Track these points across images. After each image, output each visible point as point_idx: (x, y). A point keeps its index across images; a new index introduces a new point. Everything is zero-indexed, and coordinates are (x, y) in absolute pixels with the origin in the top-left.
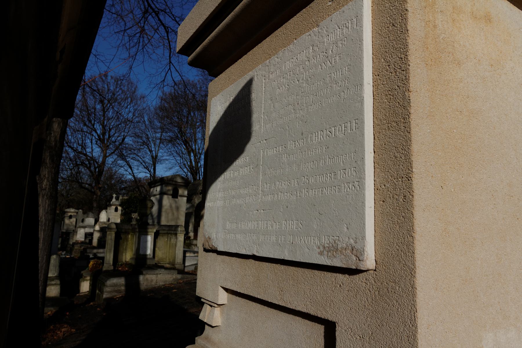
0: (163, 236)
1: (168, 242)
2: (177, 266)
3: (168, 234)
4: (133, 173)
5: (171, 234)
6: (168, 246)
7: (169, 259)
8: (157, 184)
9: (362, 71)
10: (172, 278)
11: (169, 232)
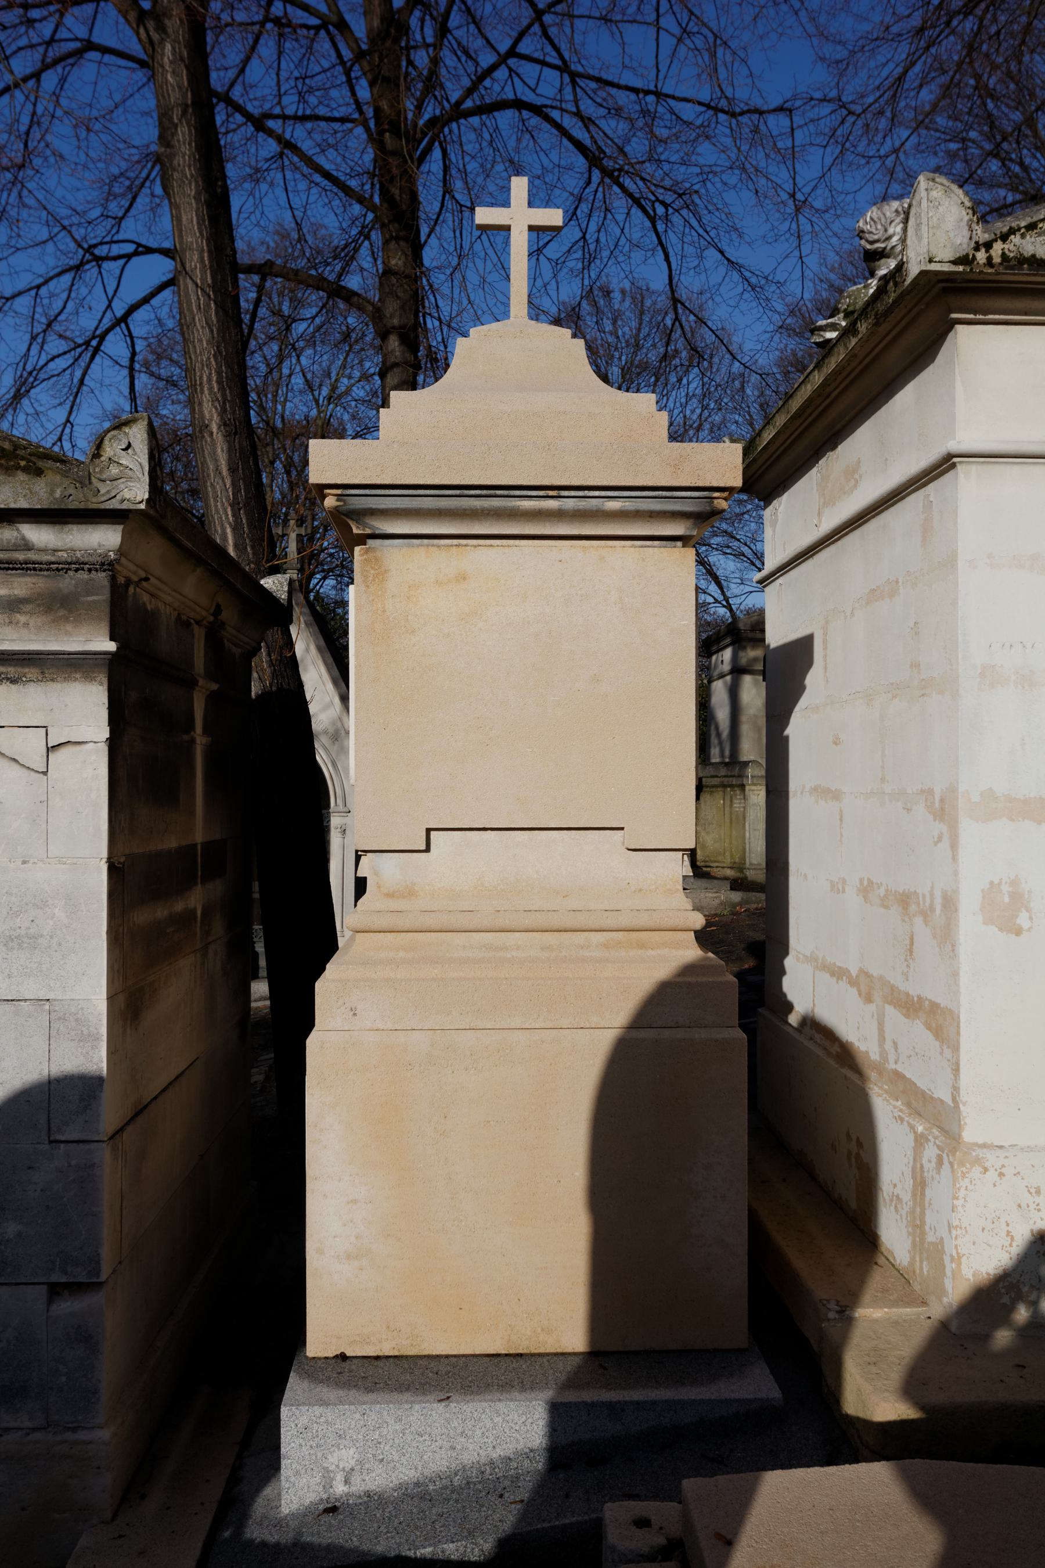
0: (711, 793)
1: (727, 809)
4: (726, 599)
5: (732, 786)
6: (727, 820)
7: (732, 856)
8: (722, 644)
9: (347, 657)
10: (717, 901)
11: (726, 780)
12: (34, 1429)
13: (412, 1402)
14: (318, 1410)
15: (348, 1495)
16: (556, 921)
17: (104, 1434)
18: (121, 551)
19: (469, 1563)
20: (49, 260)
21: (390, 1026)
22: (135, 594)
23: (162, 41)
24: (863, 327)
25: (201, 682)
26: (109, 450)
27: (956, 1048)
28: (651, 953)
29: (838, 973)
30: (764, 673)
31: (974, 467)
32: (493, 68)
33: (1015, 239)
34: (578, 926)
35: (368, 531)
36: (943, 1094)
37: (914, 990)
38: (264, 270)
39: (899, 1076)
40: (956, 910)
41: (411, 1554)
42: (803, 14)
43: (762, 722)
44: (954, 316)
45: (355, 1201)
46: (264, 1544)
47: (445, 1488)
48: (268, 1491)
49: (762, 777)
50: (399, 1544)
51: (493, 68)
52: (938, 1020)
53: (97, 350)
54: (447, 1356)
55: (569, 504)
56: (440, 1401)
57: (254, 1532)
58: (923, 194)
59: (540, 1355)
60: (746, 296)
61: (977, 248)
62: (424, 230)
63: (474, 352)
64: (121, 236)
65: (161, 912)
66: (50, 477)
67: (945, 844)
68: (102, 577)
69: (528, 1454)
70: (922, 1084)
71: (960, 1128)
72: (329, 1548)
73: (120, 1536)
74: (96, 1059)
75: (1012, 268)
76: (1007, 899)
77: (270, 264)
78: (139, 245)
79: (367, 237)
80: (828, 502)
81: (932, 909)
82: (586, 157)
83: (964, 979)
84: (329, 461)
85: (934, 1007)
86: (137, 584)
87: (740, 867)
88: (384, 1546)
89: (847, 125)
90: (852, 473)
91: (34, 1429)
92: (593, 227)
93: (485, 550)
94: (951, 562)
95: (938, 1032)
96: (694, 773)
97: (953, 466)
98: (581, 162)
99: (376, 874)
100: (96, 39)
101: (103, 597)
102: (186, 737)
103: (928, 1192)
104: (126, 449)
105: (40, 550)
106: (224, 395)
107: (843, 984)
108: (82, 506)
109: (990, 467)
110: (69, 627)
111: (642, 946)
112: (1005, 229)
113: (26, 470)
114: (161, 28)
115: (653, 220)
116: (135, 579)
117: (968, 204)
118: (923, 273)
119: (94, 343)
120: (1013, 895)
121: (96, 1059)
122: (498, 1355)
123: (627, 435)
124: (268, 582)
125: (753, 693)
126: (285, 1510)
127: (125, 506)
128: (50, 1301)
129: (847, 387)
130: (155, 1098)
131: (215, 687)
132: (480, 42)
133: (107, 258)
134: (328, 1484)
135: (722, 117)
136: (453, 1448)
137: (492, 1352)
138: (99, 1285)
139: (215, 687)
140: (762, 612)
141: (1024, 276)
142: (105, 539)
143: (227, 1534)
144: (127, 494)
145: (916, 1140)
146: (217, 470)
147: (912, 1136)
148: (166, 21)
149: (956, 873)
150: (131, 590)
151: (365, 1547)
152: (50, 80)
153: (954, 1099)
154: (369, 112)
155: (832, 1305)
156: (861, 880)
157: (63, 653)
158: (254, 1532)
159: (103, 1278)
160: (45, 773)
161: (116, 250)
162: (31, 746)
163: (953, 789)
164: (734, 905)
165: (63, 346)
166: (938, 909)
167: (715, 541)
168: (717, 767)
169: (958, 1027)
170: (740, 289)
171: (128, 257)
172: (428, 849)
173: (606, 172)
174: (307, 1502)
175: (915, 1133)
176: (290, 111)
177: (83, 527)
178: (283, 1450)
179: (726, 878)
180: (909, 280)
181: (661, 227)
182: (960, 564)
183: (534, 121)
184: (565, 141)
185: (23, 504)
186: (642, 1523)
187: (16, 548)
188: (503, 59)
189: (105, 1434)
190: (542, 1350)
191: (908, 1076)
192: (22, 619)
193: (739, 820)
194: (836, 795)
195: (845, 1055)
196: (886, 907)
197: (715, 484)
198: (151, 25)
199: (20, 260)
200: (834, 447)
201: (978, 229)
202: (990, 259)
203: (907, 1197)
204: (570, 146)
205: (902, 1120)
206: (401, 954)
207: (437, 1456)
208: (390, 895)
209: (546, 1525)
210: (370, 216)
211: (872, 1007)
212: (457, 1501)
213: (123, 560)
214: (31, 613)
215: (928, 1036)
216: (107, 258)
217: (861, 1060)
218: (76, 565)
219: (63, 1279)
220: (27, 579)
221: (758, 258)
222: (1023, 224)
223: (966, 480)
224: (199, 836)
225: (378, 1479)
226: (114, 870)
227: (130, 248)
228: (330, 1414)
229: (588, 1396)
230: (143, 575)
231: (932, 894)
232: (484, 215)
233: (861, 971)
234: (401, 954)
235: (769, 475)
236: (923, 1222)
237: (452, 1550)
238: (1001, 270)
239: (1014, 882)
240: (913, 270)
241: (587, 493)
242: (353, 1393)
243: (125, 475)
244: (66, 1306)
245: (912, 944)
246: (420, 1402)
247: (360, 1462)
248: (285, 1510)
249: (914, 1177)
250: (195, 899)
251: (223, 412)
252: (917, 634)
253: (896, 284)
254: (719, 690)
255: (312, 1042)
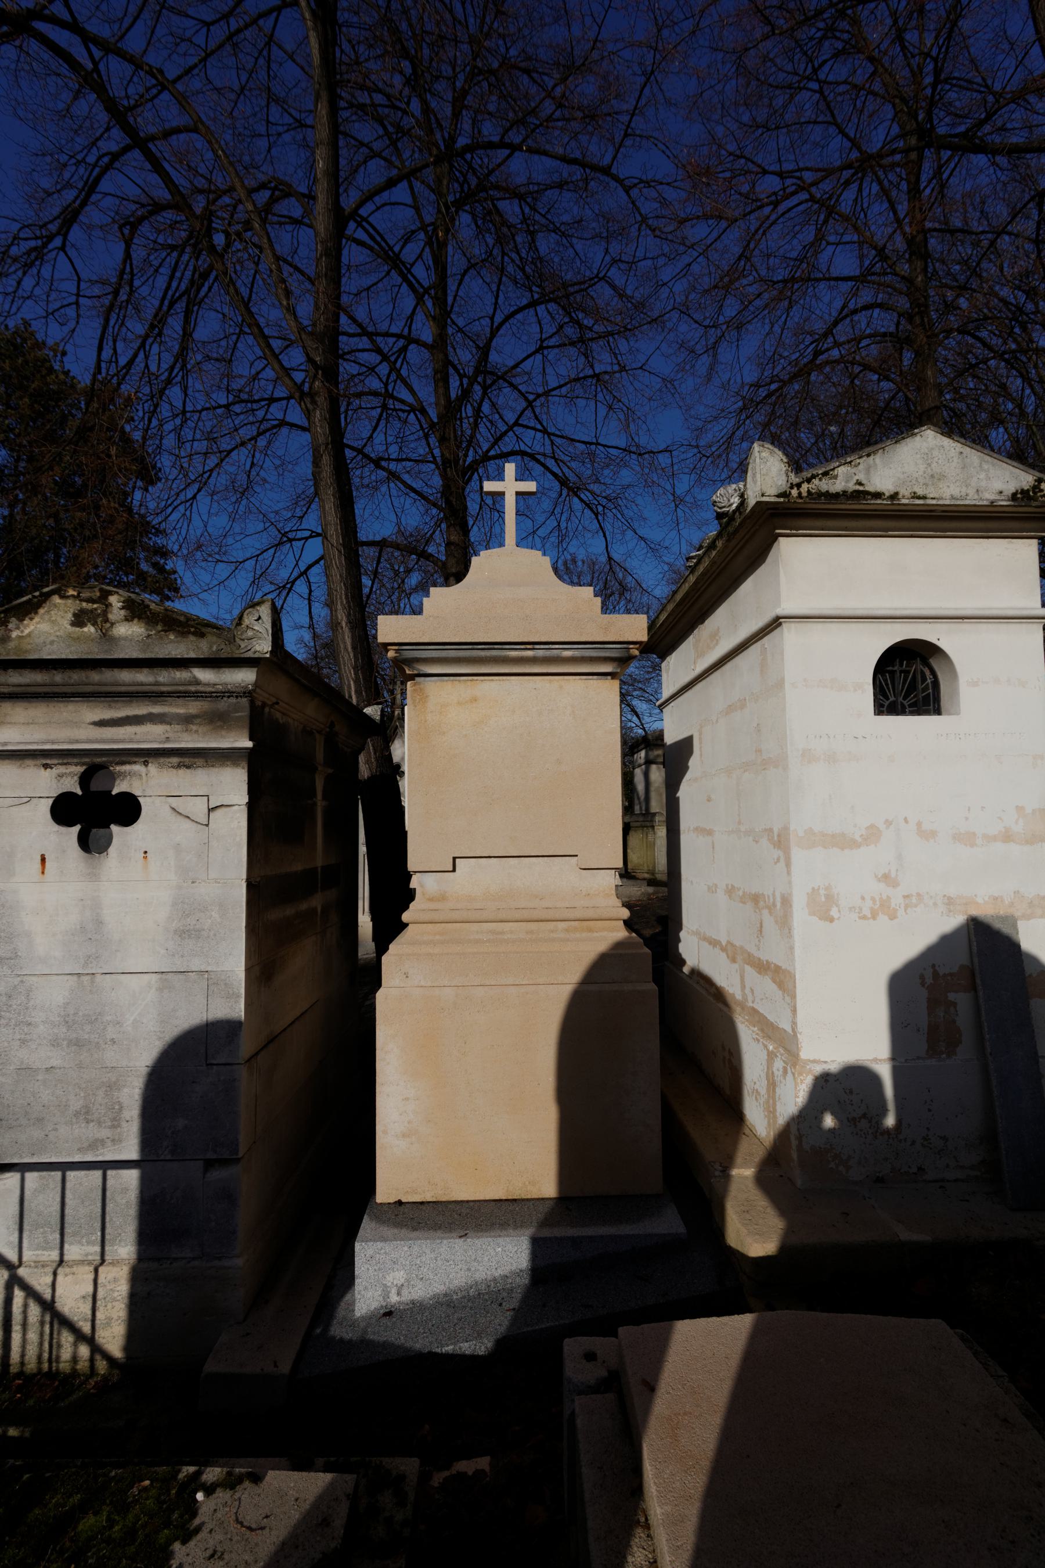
2: (659, 877)
3: (643, 827)
12: (194, 1259)
13: (442, 1238)
14: (380, 1245)
15: (399, 1303)
16: (536, 915)
17: (240, 1262)
18: (256, 684)
19: (478, 1356)
20: (265, 540)
21: (429, 984)
22: (270, 712)
23: (315, 409)
24: (719, 544)
25: (320, 768)
26: (246, 621)
27: (793, 997)
28: (595, 934)
29: (714, 943)
30: (663, 763)
31: (793, 625)
32: (506, 432)
33: (816, 481)
34: (549, 918)
35: (416, 672)
36: (785, 1025)
37: (764, 956)
38: (382, 544)
39: (755, 1011)
40: (791, 906)
41: (438, 1350)
42: (676, 395)
43: (663, 790)
44: (778, 531)
45: (407, 1099)
46: (341, 1340)
47: (464, 1297)
48: (348, 1297)
49: (884, 1060)
50: (431, 1343)
51: (506, 432)
52: (782, 978)
53: (290, 589)
54: (468, 1201)
55: (540, 653)
56: (461, 1237)
57: (337, 1331)
58: (757, 454)
59: (528, 1200)
60: (649, 555)
61: (792, 487)
62: (471, 523)
63: (482, 563)
64: (302, 527)
65: (289, 911)
66: (211, 638)
67: (782, 863)
68: (244, 701)
69: (519, 1273)
70: (771, 1018)
71: (798, 1049)
72: (385, 1345)
73: (248, 1334)
74: (237, 1009)
75: (814, 499)
76: (823, 899)
77: (384, 540)
78: (313, 532)
79: (440, 526)
80: (700, 655)
81: (774, 905)
82: (559, 481)
83: (798, 952)
84: (391, 628)
85: (778, 969)
86: (271, 706)
87: (652, 872)
88: (421, 1344)
89: (703, 461)
90: (715, 637)
91: (194, 1259)
92: (564, 518)
93: (488, 683)
94: (780, 684)
95: (781, 985)
96: (620, 818)
97: (780, 624)
98: (556, 485)
99: (422, 886)
100: (288, 419)
101: (245, 713)
102: (310, 802)
103: (777, 1090)
104: (257, 620)
105: (205, 685)
106: (349, 607)
107: (717, 950)
108: (229, 656)
109: (803, 625)
110: (223, 733)
111: (590, 930)
112: (809, 475)
113: (195, 634)
114: (314, 402)
115: (596, 514)
116: (270, 703)
117: (785, 460)
118: (758, 503)
119: (289, 586)
120: (827, 896)
121: (237, 1009)
122: (501, 1200)
123: (576, 612)
124: (368, 711)
125: (657, 775)
126: (358, 1314)
127: (256, 655)
128: (206, 1170)
129: (710, 584)
130: (285, 1029)
131: (330, 771)
132: (497, 416)
133: (294, 540)
134: (386, 1295)
135: (634, 456)
136: (469, 1270)
137: (497, 1198)
138: (238, 1160)
139: (330, 771)
140: (662, 731)
141: (822, 505)
142: (246, 677)
143: (318, 1331)
144: (258, 648)
145: (768, 1055)
146: (346, 649)
147: (765, 1052)
148: (317, 399)
149: (790, 883)
150: (267, 710)
151: (408, 1345)
152: (262, 442)
153: (793, 1030)
154: (439, 459)
155: (717, 1166)
156: (727, 885)
157: (220, 749)
158: (337, 1331)
159: (240, 1155)
160: (207, 825)
161: (300, 535)
162: (198, 809)
163: (786, 828)
164: (649, 894)
165: (273, 588)
166: (779, 905)
167: (635, 693)
168: (636, 816)
169: (795, 982)
170: (645, 551)
171: (306, 539)
172: (454, 870)
173: (570, 489)
174: (372, 1308)
175: (768, 1050)
176: (394, 456)
177: (232, 670)
178: (356, 1273)
179: (644, 879)
180: (749, 509)
181: (600, 518)
182: (787, 685)
183: (532, 464)
184: (548, 474)
185: (192, 655)
186: (590, 1357)
187: (190, 684)
188: (511, 428)
189: (239, 1262)
190: (529, 1197)
191: (761, 1011)
192: (194, 728)
193: (651, 846)
194: (710, 833)
195: (719, 995)
196: (744, 903)
197: (630, 639)
198: (308, 400)
199: (247, 541)
200: (703, 622)
201: (792, 475)
202: (800, 494)
203: (763, 1091)
204: (551, 477)
205: (758, 1041)
206: (438, 937)
207: (459, 1275)
208: (431, 900)
209: (529, 1329)
210: (442, 515)
211: (736, 966)
212: (471, 1308)
213: (258, 690)
214: (200, 724)
215: (774, 987)
216: (294, 540)
217: (729, 999)
218: (228, 693)
219: (215, 1157)
220: (198, 703)
221: (655, 535)
222: (820, 472)
223: (789, 633)
224: (319, 862)
225: (419, 1292)
226: (251, 886)
227: (307, 534)
228: (387, 1247)
229: (559, 1232)
230: (274, 700)
231: (774, 895)
232: (489, 486)
233: (728, 942)
234: (438, 937)
235: (663, 641)
236: (775, 1110)
237: (467, 1347)
238: (808, 500)
239: (828, 888)
240: (751, 502)
241: (551, 646)
242: (404, 1231)
243: (257, 636)
244: (216, 1174)
245: (761, 926)
246: (447, 1238)
247: (408, 1281)
248: (358, 1314)
249: (768, 1079)
250: (316, 902)
251: (349, 615)
252: (759, 731)
253: (740, 514)
254: (638, 773)
255: (380, 995)
